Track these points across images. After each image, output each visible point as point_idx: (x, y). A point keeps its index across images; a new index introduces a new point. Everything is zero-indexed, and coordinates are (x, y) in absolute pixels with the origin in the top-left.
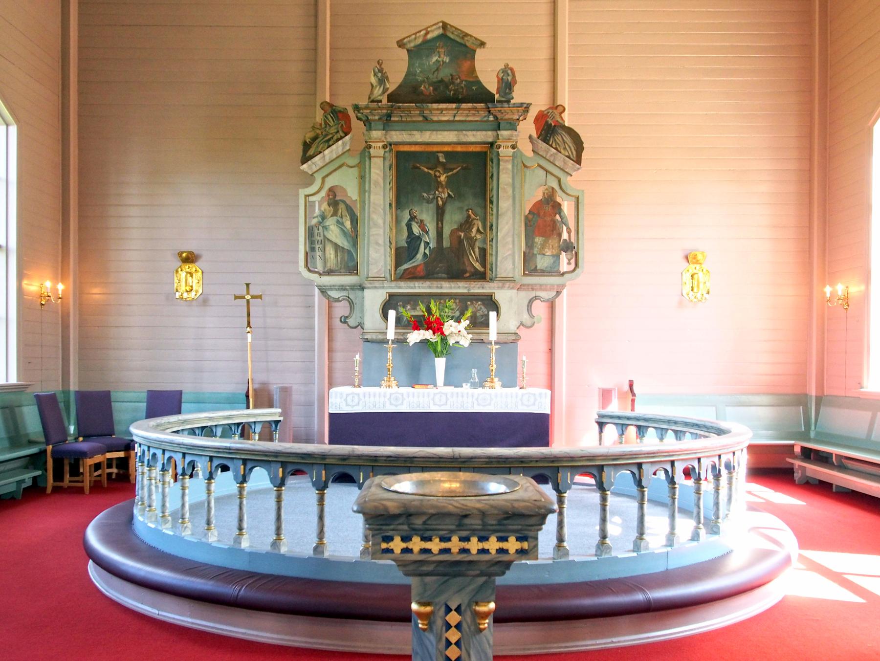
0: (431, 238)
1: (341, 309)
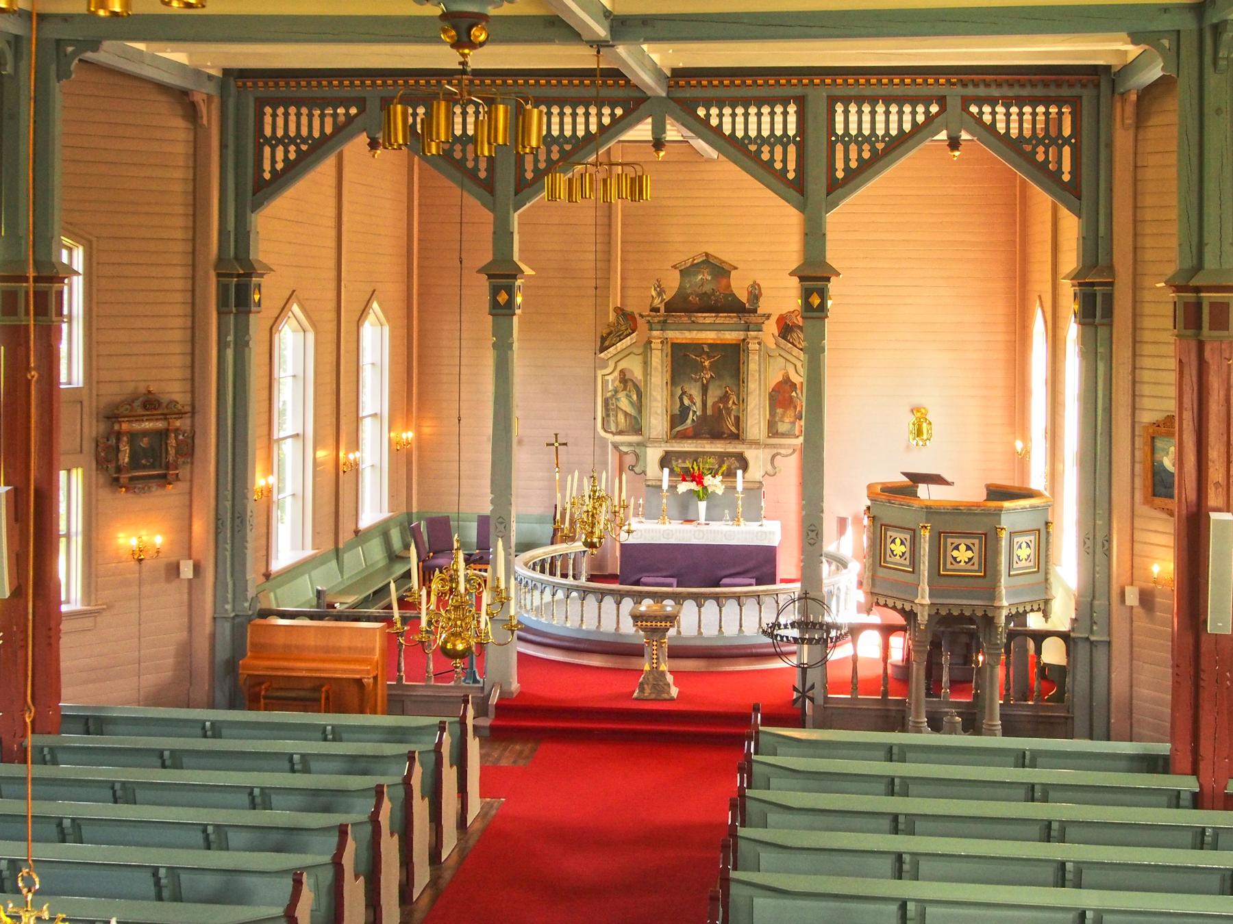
0: (697, 408)
1: (630, 460)
